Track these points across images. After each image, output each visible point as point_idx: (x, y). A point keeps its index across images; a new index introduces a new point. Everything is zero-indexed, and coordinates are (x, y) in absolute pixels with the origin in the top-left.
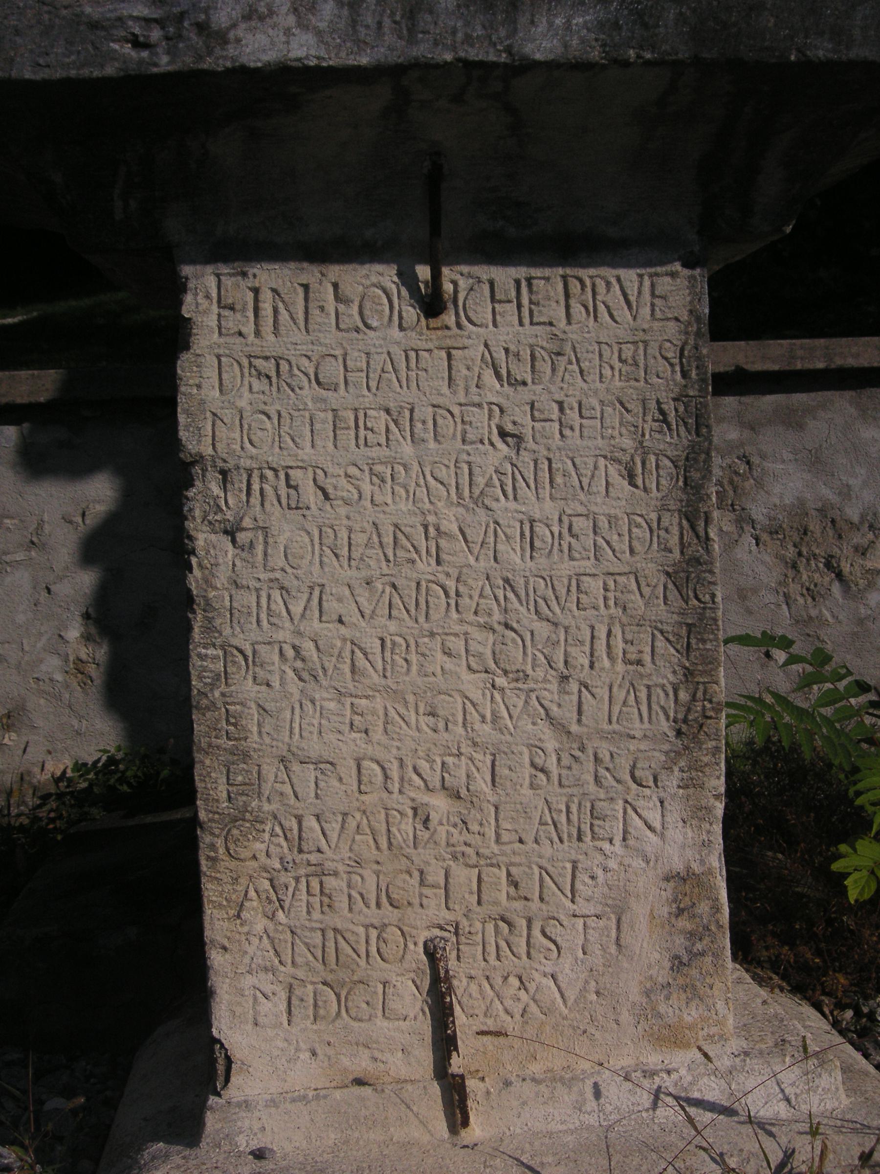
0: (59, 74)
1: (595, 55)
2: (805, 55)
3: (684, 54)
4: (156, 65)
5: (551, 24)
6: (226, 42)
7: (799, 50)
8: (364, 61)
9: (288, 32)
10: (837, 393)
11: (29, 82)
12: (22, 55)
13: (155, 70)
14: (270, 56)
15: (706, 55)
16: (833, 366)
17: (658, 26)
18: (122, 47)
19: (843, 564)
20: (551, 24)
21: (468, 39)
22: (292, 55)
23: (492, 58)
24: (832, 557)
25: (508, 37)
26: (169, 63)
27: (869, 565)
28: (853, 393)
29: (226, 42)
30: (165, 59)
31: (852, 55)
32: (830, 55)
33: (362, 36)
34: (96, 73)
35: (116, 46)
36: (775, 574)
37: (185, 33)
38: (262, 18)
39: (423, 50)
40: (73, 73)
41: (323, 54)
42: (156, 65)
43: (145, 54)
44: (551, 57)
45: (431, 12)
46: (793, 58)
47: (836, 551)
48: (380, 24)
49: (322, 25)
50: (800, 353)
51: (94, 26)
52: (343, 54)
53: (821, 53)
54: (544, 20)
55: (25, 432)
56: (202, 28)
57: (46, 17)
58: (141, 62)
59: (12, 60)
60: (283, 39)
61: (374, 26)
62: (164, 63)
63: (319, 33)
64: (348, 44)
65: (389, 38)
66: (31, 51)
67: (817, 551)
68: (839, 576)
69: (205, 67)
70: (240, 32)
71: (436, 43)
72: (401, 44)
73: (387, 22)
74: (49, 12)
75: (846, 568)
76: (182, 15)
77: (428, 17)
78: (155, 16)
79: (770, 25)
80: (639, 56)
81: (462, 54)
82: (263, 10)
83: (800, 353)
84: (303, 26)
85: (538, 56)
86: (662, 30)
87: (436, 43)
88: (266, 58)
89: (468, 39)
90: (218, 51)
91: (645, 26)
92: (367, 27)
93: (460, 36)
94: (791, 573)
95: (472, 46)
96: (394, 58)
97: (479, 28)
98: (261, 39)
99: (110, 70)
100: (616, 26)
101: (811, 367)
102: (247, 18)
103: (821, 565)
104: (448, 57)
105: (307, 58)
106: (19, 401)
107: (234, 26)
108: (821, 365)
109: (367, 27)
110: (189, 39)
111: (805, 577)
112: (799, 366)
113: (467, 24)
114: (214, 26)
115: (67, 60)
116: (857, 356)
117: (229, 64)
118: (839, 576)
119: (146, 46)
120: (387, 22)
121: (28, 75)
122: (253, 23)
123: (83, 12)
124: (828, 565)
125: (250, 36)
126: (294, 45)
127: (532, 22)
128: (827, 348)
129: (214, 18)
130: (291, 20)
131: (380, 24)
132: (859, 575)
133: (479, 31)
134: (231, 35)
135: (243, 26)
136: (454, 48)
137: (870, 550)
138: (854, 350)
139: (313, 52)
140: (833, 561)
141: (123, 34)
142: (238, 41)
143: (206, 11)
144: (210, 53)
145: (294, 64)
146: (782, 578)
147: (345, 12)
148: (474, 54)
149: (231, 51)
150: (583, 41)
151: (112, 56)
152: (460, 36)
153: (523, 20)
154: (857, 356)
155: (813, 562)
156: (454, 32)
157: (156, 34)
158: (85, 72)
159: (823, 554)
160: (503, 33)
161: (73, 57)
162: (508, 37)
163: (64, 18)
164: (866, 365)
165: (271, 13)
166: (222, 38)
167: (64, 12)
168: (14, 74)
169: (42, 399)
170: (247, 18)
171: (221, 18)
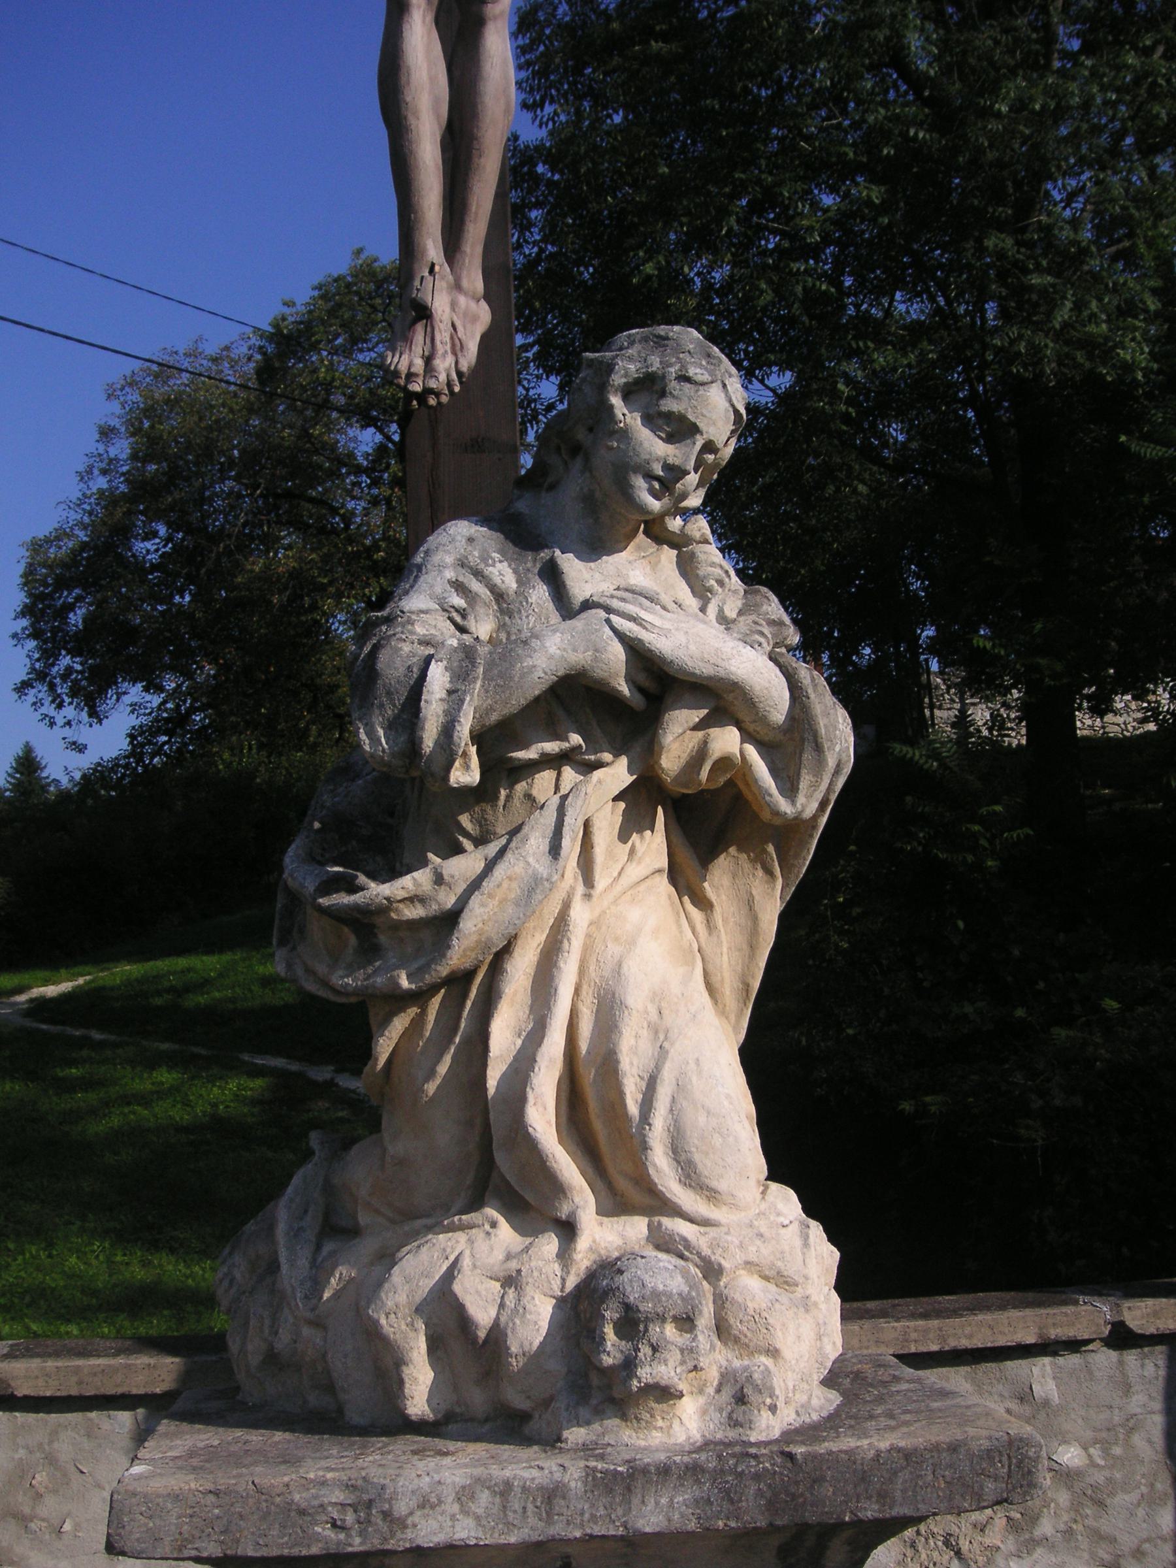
0: (275, 1552)
1: (692, 1526)
2: (856, 1516)
3: (762, 1523)
4: (350, 1545)
5: (657, 1503)
6: (405, 1527)
7: (851, 1512)
8: (513, 1540)
9: (453, 1517)
10: (952, 1370)
11: (251, 1557)
12: (246, 1537)
13: (350, 1549)
14: (439, 1538)
15: (779, 1522)
16: (947, 1348)
17: (740, 1501)
18: (324, 1529)
19: (961, 1542)
20: (657, 1503)
21: (594, 1518)
22: (457, 1536)
23: (612, 1532)
24: (951, 1535)
25: (624, 1515)
26: (361, 1544)
27: (988, 1541)
28: (968, 1369)
29: (405, 1527)
30: (358, 1540)
31: (894, 1513)
32: (876, 1515)
33: (511, 1519)
34: (304, 1553)
35: (318, 1529)
36: (893, 1554)
37: (373, 1519)
38: (433, 1507)
39: (559, 1529)
40: (286, 1552)
41: (481, 1535)
42: (350, 1545)
43: (342, 1536)
44: (657, 1529)
45: (564, 1498)
46: (847, 1519)
47: (954, 1529)
48: (524, 1508)
49: (480, 1511)
50: (914, 1335)
51: (302, 1512)
52: (496, 1535)
53: (869, 1514)
54: (652, 1501)
55: (140, 1417)
56: (386, 1515)
57: (264, 1504)
58: (339, 1543)
59: (238, 1541)
60: (450, 1524)
61: (520, 1511)
62: (357, 1544)
63: (478, 1518)
64: (500, 1526)
65: (532, 1520)
66: (253, 1533)
67: (935, 1530)
68: (958, 1553)
69: (389, 1547)
70: (416, 1518)
71: (568, 1523)
72: (541, 1524)
73: (530, 1507)
74: (266, 1501)
75: (965, 1546)
76: (370, 1504)
77: (562, 1502)
78: (349, 1502)
79: (830, 1494)
80: (726, 1525)
81: (589, 1531)
82: (434, 1500)
83: (914, 1335)
84: (465, 1512)
85: (648, 1530)
86: (744, 1504)
87: (568, 1523)
88: (436, 1539)
89: (594, 1518)
90: (399, 1535)
91: (731, 1501)
92: (515, 1512)
93: (587, 1516)
94: (910, 1552)
95: (596, 1523)
96: (536, 1537)
97: (601, 1508)
98: (433, 1524)
99: (315, 1550)
100: (709, 1502)
101: (925, 1350)
102: (421, 1506)
103: (940, 1544)
104: (578, 1534)
105: (468, 1538)
106: (135, 1391)
107: (411, 1514)
108: (935, 1348)
109: (515, 1512)
110: (376, 1524)
111: (924, 1556)
112: (913, 1350)
113: (592, 1506)
114: (396, 1514)
115: (281, 1541)
116: (970, 1337)
117: (408, 1545)
118: (958, 1553)
119: (343, 1528)
120: (530, 1507)
121: (250, 1553)
122: (426, 1511)
123: (292, 1501)
124: (947, 1543)
125: (423, 1522)
126: (458, 1528)
127: (643, 1502)
128: (940, 1329)
129: (395, 1508)
130: (456, 1507)
131: (524, 1508)
132: (978, 1552)
133: (602, 1512)
134: (409, 1521)
135: (419, 1513)
136: (582, 1526)
137: (988, 1527)
138: (968, 1330)
139: (473, 1534)
140: (952, 1539)
141: (325, 1518)
142: (415, 1526)
143: (390, 1501)
144: (393, 1534)
145: (457, 1543)
146: (901, 1557)
147: (498, 1500)
148: (598, 1530)
149: (409, 1534)
150: (682, 1515)
151: (317, 1538)
152: (587, 1516)
153: (636, 1501)
154: (970, 1337)
155: (931, 1541)
156: (582, 1514)
157: (350, 1518)
158: (295, 1552)
159: (941, 1532)
160: (620, 1511)
161: (286, 1539)
162: (624, 1515)
163: (278, 1506)
164: (980, 1346)
165: (440, 1502)
166: (402, 1523)
167: (278, 1500)
168: (240, 1552)
169: (158, 1391)
170: (421, 1506)
171: (401, 1507)
